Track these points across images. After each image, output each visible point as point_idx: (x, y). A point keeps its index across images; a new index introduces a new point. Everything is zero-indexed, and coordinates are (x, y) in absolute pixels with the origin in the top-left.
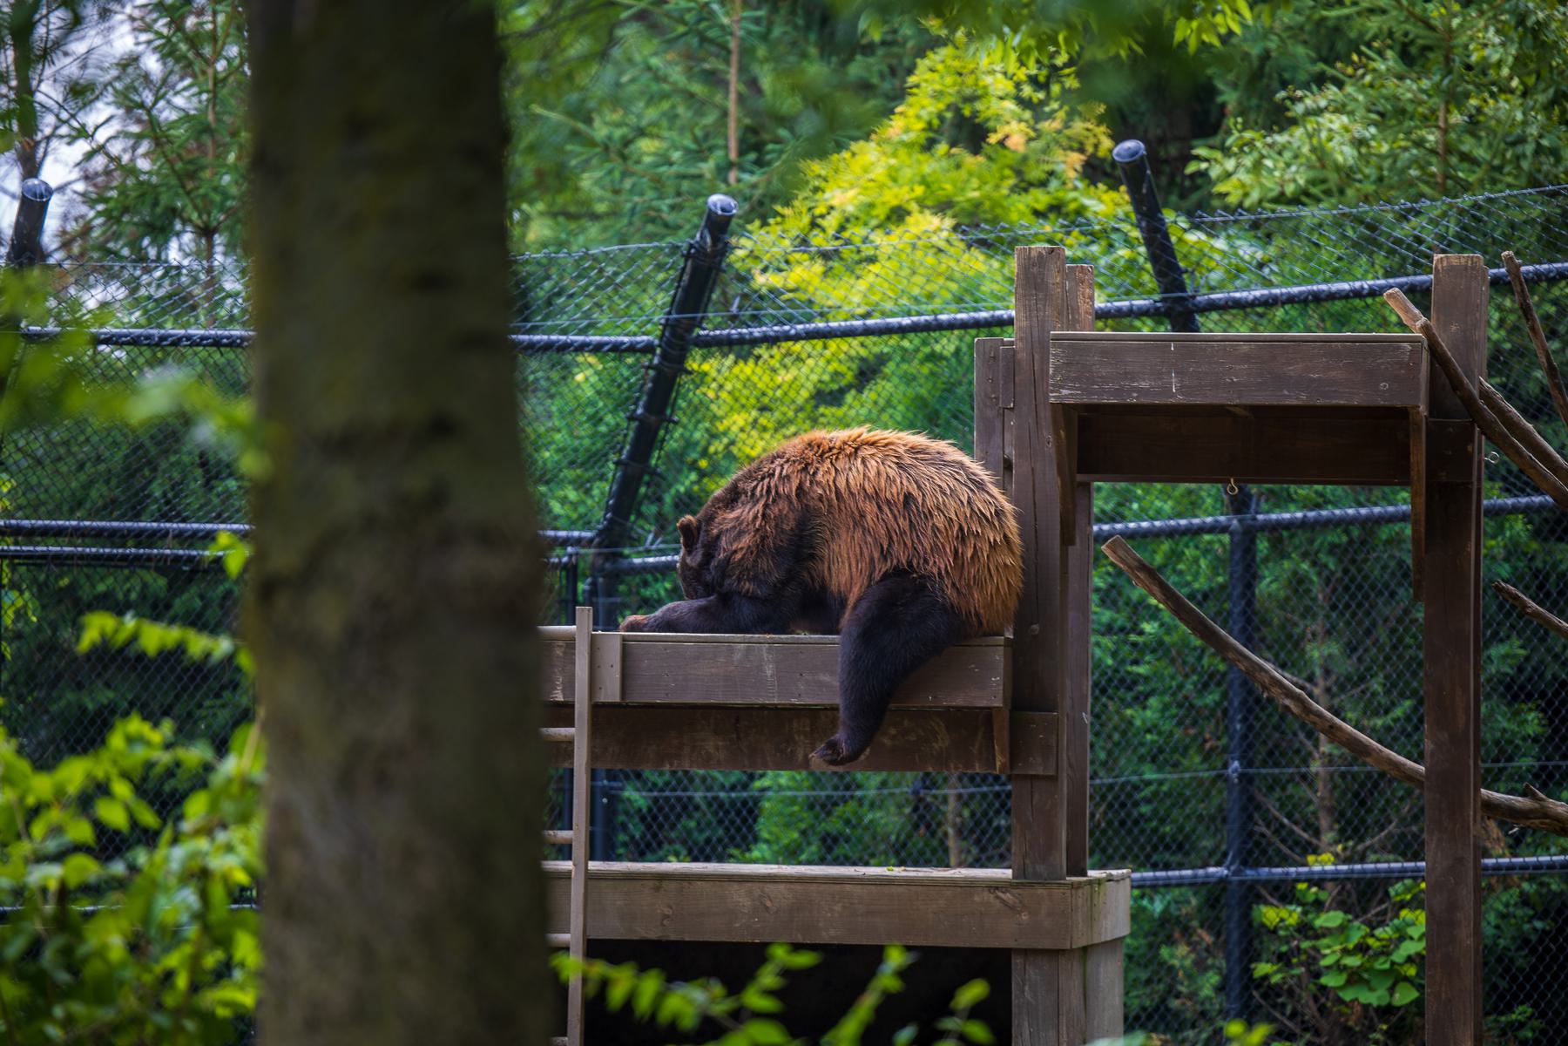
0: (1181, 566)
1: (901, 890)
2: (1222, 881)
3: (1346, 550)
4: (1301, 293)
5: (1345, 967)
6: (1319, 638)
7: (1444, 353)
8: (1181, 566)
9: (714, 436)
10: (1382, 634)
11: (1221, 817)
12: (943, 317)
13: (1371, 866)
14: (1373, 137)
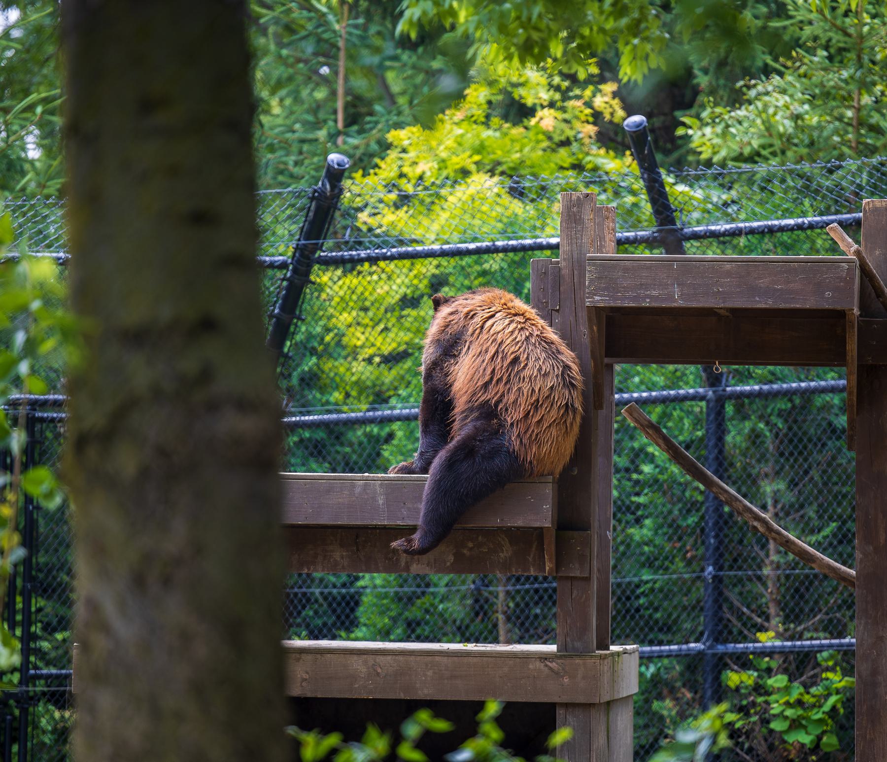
0: (670, 424)
1: (475, 660)
2: (700, 653)
3: (790, 413)
4: (759, 227)
5: (786, 718)
6: (770, 477)
7: (871, 270)
8: (670, 424)
9: (328, 330)
10: (815, 474)
11: (697, 607)
12: (499, 243)
13: (808, 643)
14: (807, 113)
